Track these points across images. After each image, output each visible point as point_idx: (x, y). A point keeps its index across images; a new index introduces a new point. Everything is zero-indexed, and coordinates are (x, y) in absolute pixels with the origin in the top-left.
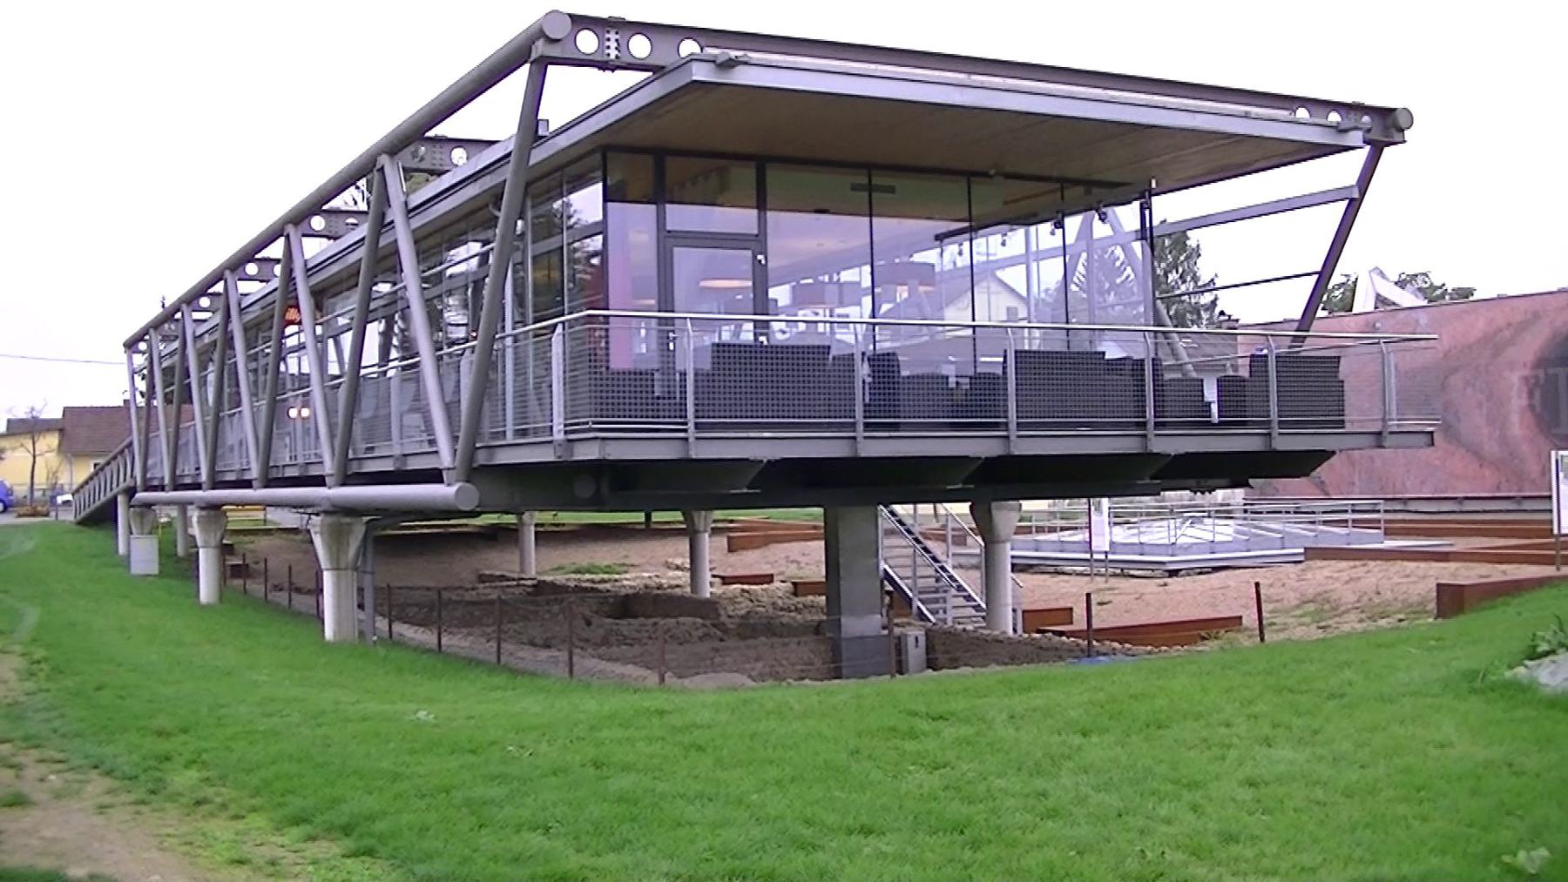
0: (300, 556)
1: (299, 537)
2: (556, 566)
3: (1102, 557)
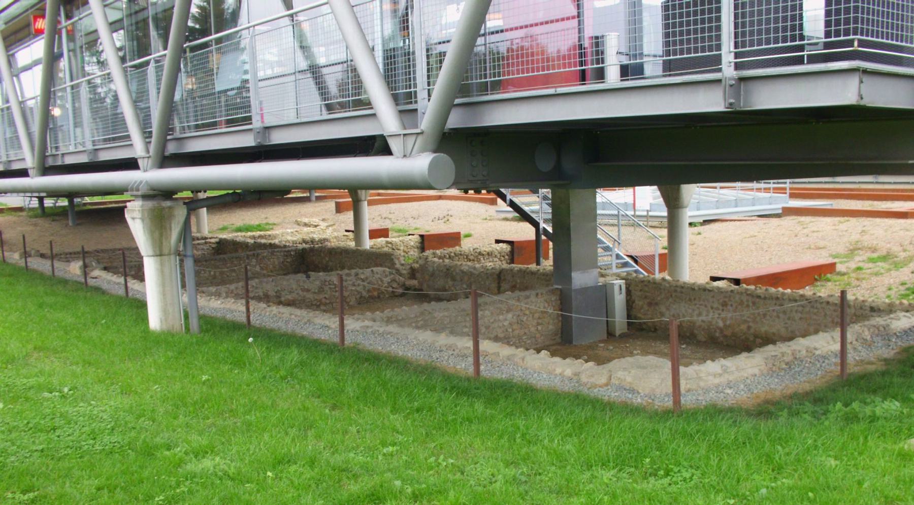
0: (31, 228)
1: (24, 214)
2: (221, 227)
3: (645, 213)
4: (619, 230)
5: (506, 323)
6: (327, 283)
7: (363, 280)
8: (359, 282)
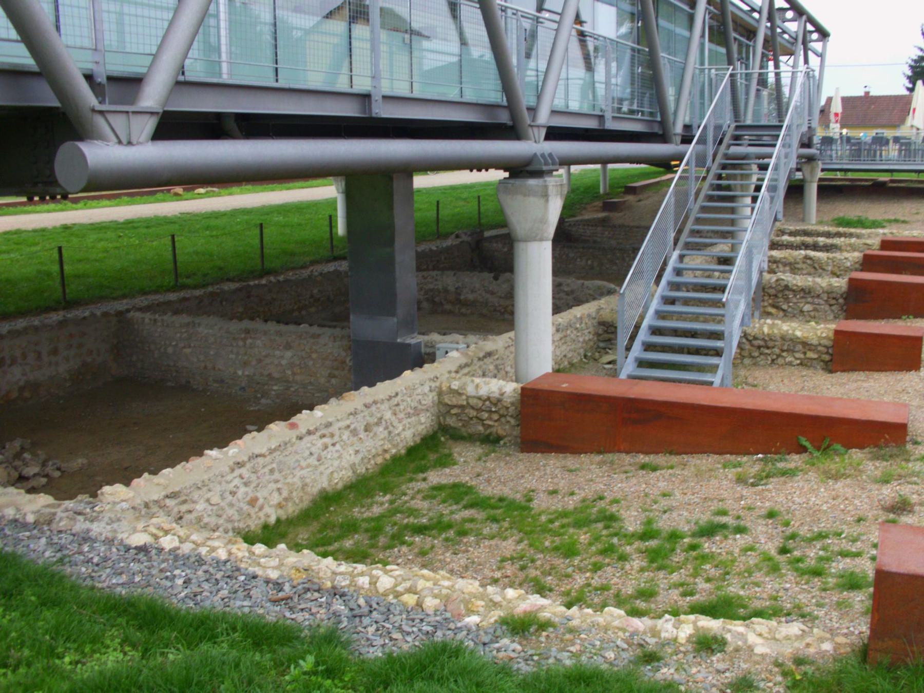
5: (284, 362)
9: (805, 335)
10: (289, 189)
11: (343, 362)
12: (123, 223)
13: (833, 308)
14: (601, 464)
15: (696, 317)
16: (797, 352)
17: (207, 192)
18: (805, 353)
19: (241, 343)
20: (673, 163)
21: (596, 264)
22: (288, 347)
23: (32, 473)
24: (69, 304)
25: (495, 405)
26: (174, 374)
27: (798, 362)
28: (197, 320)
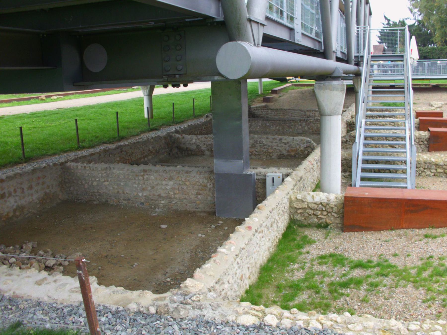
4: (118, 134)
6: (258, 142)
7: (285, 144)
8: (283, 145)
9: (437, 160)
10: (99, 96)
11: (206, 186)
12: (30, 115)
13: (422, 146)
14: (400, 236)
15: (377, 153)
16: (432, 169)
17: (58, 98)
18: (436, 170)
19: (141, 178)
20: (288, 78)
21: (281, 128)
22: (171, 179)
23: (52, 264)
24: (27, 160)
25: (325, 207)
26: (98, 197)
27: (433, 174)
28: (112, 166)
